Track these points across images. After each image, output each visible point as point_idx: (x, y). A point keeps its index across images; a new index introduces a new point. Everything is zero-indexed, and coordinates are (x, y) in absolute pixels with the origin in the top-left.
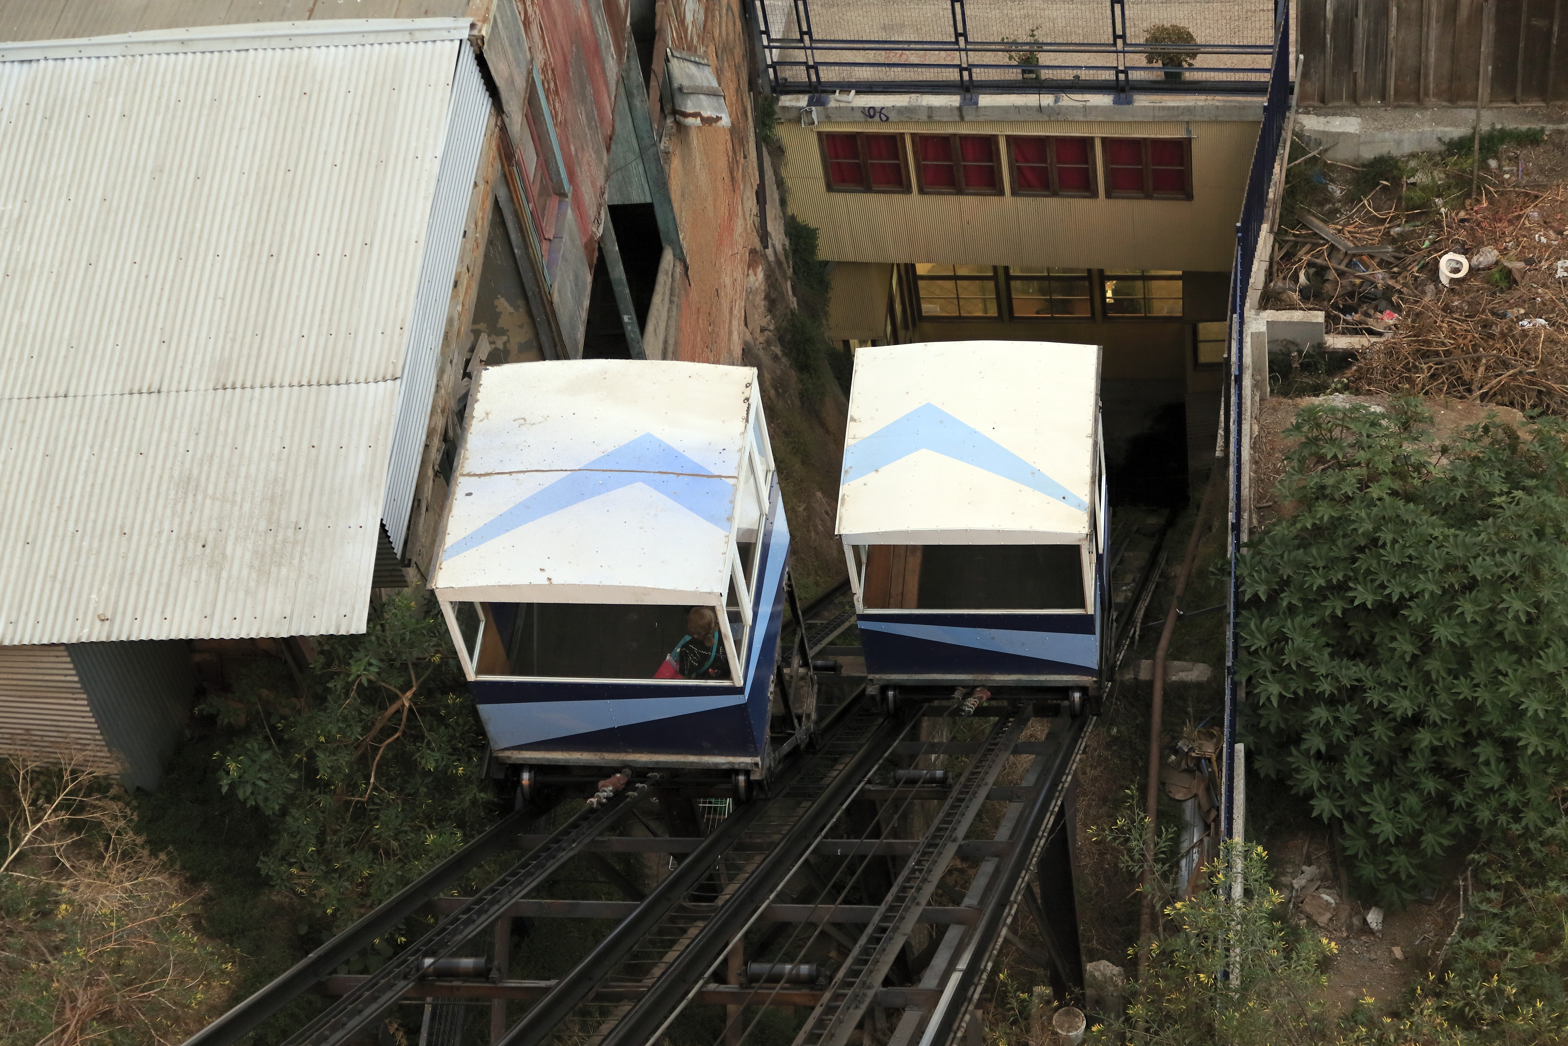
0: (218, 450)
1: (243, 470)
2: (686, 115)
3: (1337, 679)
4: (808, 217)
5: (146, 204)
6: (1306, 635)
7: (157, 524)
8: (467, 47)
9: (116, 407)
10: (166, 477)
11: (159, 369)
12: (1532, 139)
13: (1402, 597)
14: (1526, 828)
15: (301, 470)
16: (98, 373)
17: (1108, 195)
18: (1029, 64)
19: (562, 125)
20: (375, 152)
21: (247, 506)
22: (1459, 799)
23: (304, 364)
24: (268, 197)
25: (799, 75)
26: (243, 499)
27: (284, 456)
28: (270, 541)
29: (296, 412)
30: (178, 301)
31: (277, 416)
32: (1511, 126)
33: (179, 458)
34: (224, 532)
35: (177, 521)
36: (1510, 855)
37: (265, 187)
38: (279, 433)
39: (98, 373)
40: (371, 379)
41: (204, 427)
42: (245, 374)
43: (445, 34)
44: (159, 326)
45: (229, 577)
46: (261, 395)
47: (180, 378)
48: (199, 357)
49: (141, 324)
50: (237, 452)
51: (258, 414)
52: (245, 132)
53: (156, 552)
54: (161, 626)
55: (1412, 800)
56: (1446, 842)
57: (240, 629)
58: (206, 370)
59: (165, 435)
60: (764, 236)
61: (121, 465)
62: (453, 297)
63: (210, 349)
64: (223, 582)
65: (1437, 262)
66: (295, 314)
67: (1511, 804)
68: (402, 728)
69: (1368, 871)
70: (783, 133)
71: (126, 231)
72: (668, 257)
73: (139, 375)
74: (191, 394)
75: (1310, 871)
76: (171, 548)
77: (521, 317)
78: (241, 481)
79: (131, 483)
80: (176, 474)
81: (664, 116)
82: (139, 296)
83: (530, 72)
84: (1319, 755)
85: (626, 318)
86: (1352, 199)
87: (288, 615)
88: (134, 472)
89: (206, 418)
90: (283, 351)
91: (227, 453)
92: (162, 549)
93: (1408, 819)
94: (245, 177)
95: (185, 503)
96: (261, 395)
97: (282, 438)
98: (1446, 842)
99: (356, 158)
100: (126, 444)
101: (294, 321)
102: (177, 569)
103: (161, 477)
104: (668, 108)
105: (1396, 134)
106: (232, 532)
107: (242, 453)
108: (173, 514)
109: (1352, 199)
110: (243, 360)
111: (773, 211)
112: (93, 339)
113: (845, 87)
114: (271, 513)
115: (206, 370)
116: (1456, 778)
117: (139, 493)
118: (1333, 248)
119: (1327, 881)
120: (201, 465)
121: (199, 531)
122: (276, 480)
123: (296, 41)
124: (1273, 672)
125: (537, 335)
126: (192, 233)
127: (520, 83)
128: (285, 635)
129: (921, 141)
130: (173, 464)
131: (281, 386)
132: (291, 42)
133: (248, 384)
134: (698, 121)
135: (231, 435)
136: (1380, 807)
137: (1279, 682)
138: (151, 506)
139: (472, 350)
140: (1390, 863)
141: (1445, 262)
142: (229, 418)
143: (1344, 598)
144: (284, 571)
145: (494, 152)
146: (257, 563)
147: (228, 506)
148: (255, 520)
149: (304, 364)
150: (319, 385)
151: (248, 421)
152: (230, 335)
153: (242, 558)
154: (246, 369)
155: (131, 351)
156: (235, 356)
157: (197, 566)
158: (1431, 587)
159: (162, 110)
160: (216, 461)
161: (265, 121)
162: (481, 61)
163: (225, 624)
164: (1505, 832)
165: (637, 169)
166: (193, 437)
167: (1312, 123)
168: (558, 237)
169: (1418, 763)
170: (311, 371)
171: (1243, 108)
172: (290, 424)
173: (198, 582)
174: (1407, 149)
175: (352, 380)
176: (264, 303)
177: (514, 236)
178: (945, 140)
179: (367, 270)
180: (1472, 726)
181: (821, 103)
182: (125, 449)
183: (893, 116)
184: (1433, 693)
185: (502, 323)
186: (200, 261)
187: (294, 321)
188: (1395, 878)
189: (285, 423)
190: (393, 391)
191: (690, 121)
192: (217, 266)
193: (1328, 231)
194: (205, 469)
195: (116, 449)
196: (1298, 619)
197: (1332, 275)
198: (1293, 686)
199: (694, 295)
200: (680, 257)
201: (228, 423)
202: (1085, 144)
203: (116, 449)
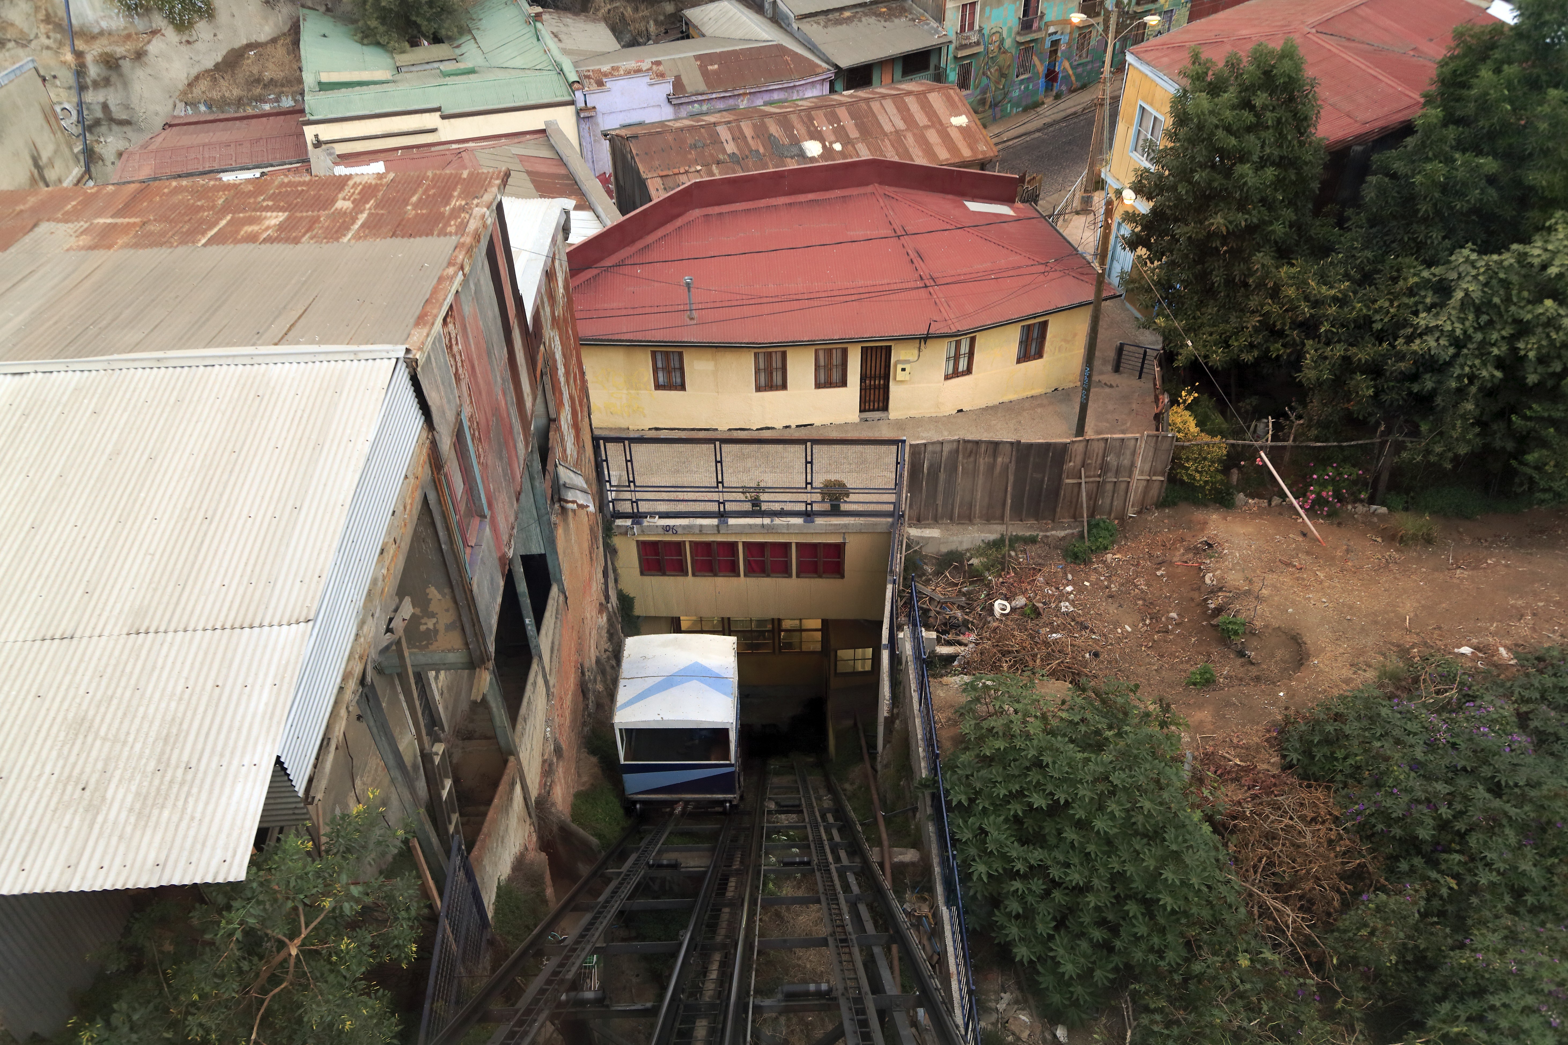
0: (119, 691)
1: (142, 710)
2: (567, 502)
3: (1025, 860)
4: (630, 590)
5: (98, 478)
6: (999, 829)
7: (38, 766)
8: (402, 366)
9: (24, 652)
10: (59, 719)
11: (76, 617)
12: (1033, 540)
13: (1066, 801)
14: (1169, 964)
15: (201, 709)
16: (15, 622)
17: (798, 576)
18: (756, 502)
19: (484, 466)
20: (314, 437)
21: (138, 746)
22: (1118, 944)
23: (220, 611)
24: (211, 472)
25: (626, 507)
26: (135, 739)
27: (186, 697)
28: (156, 782)
29: (206, 653)
30: (109, 557)
31: (185, 658)
32: (1020, 533)
33: (78, 700)
34: (108, 775)
35: (61, 762)
36: (1162, 986)
37: (211, 464)
38: (185, 674)
39: (15, 622)
40: (284, 622)
41: (110, 670)
42: (161, 620)
43: (384, 355)
44: (86, 578)
45: (105, 821)
46: (173, 638)
47: (96, 625)
48: (119, 606)
49: (69, 577)
50: (138, 693)
51: (167, 656)
52: (200, 424)
53: (31, 797)
54: (17, 877)
55: (1084, 945)
56: (1111, 976)
57: (105, 880)
58: (123, 616)
59: (68, 677)
60: (607, 597)
61: (16, 707)
62: (378, 561)
63: (131, 598)
64: (97, 828)
65: (992, 605)
66: (220, 566)
67: (1156, 947)
68: (290, 977)
69: (1056, 999)
70: (618, 541)
71: (74, 500)
72: (554, 590)
73: (55, 622)
74: (104, 639)
75: (1006, 997)
76: (48, 792)
77: (448, 602)
78: (137, 721)
79: (21, 727)
80: (71, 716)
81: (553, 502)
82: (72, 554)
83: (459, 414)
84: (1018, 916)
85: (527, 621)
86: (938, 573)
87: (161, 863)
88: (26, 716)
89: (113, 661)
90: (203, 598)
91: (128, 694)
92: (38, 793)
93: (1082, 960)
94: (193, 458)
95: (73, 744)
96: (173, 638)
97: (187, 679)
98: (1111, 976)
99: (296, 442)
100: (26, 687)
101: (217, 572)
102: (49, 814)
103: (54, 719)
104: (556, 497)
105: (960, 538)
106: (118, 773)
107: (143, 695)
108: (59, 756)
109: (938, 573)
110: (162, 607)
111: (611, 584)
112: (18, 592)
113: (652, 515)
114: (163, 752)
115: (123, 616)
116: (1115, 930)
117: (27, 735)
118: (931, 599)
119: (1020, 1003)
120: (98, 707)
121: (82, 772)
122: (173, 719)
123: (256, 360)
124: (980, 857)
125: (460, 616)
126: (135, 501)
127: (451, 416)
128: (154, 885)
129: (695, 545)
130: (70, 705)
131: (195, 630)
132: (252, 361)
133: (162, 629)
134: (575, 506)
135: (135, 677)
136: (1061, 951)
137: (985, 863)
138: (37, 748)
139: (396, 610)
140: (1072, 993)
141: (998, 605)
142: (137, 660)
143: (1021, 803)
144: (166, 813)
145: (424, 456)
146: (138, 806)
147: (118, 746)
148: (144, 761)
149: (220, 611)
150: (233, 628)
151: (155, 662)
152: (153, 585)
153: (123, 801)
154: (163, 615)
155: (53, 601)
156: (154, 604)
157: (72, 810)
158: (1088, 793)
159: (130, 409)
160: (115, 702)
161: (219, 415)
162: (415, 381)
163: (90, 874)
164: (1156, 968)
165: (535, 530)
166: (97, 679)
167: (914, 532)
168: (478, 545)
169: (1086, 919)
170: (227, 616)
171: (875, 524)
172: (197, 664)
173: (68, 828)
174: (965, 546)
175: (266, 623)
176: (192, 557)
177: (442, 534)
178: (708, 544)
179: (293, 528)
180: (1120, 890)
181: (638, 523)
182: (23, 693)
183: (680, 531)
184: (1094, 870)
185: (433, 607)
186: (138, 524)
187: (217, 572)
188: (1076, 1004)
189: (193, 664)
190: (304, 632)
191: (570, 506)
192: (153, 527)
193: (928, 590)
194: (102, 709)
195: (14, 693)
196: (992, 818)
197: (932, 614)
198: (995, 866)
199: (570, 616)
200: (562, 591)
201: (135, 665)
202: (786, 546)
203: (14, 693)
